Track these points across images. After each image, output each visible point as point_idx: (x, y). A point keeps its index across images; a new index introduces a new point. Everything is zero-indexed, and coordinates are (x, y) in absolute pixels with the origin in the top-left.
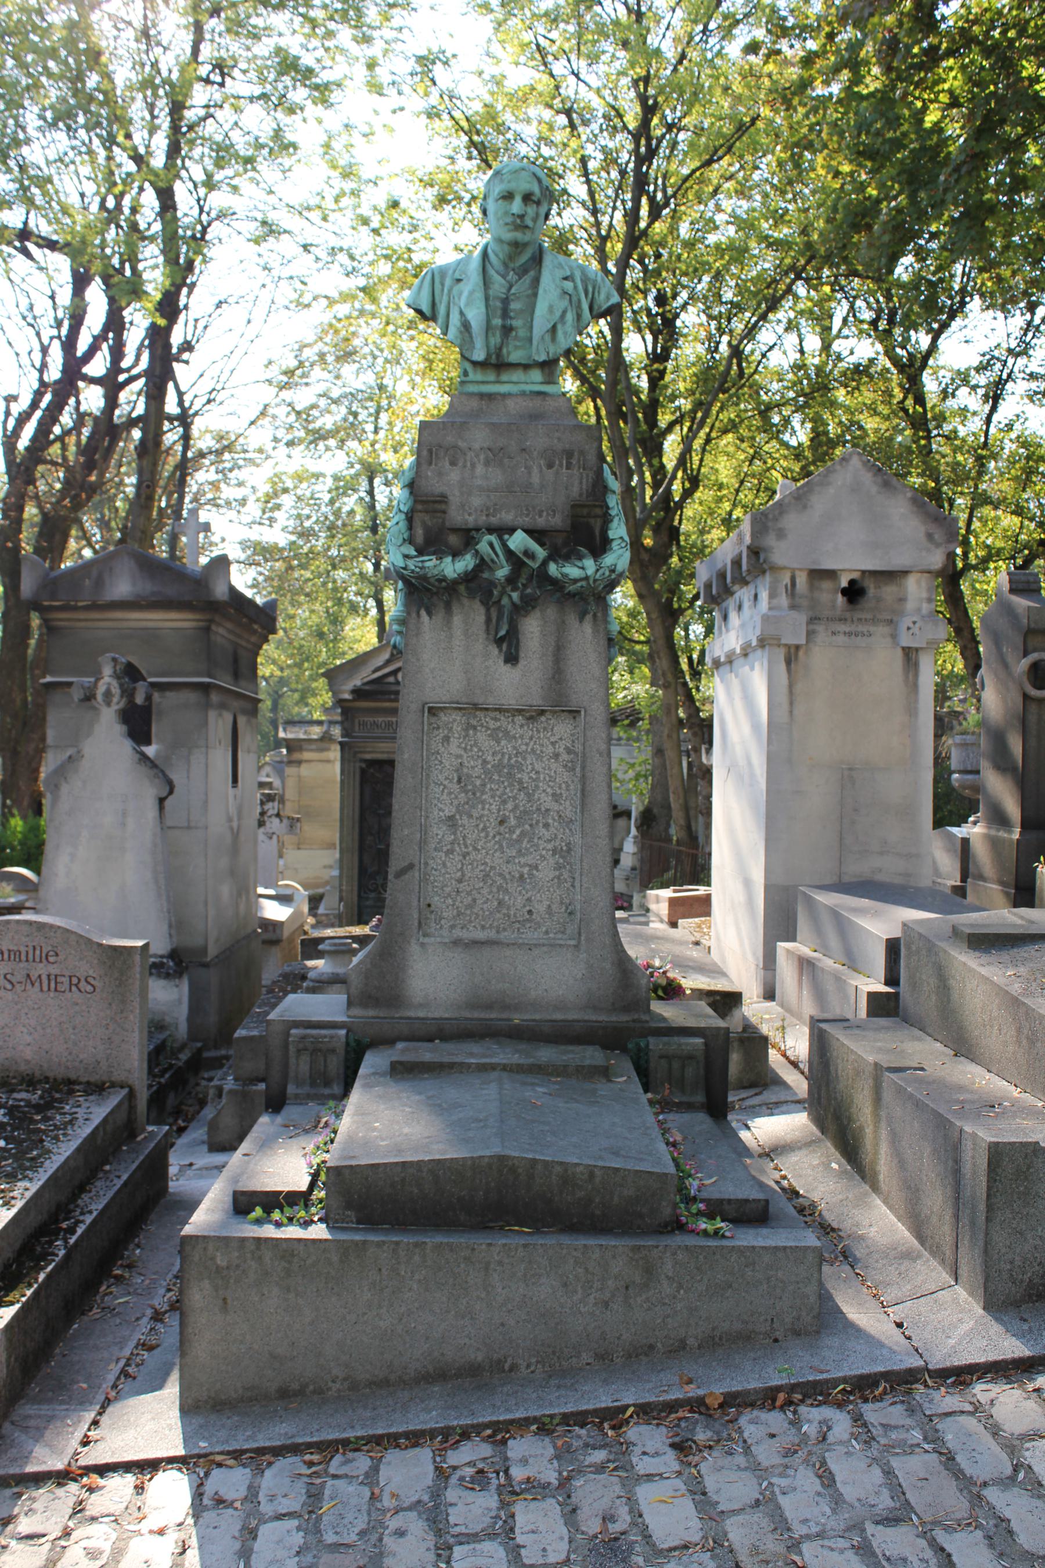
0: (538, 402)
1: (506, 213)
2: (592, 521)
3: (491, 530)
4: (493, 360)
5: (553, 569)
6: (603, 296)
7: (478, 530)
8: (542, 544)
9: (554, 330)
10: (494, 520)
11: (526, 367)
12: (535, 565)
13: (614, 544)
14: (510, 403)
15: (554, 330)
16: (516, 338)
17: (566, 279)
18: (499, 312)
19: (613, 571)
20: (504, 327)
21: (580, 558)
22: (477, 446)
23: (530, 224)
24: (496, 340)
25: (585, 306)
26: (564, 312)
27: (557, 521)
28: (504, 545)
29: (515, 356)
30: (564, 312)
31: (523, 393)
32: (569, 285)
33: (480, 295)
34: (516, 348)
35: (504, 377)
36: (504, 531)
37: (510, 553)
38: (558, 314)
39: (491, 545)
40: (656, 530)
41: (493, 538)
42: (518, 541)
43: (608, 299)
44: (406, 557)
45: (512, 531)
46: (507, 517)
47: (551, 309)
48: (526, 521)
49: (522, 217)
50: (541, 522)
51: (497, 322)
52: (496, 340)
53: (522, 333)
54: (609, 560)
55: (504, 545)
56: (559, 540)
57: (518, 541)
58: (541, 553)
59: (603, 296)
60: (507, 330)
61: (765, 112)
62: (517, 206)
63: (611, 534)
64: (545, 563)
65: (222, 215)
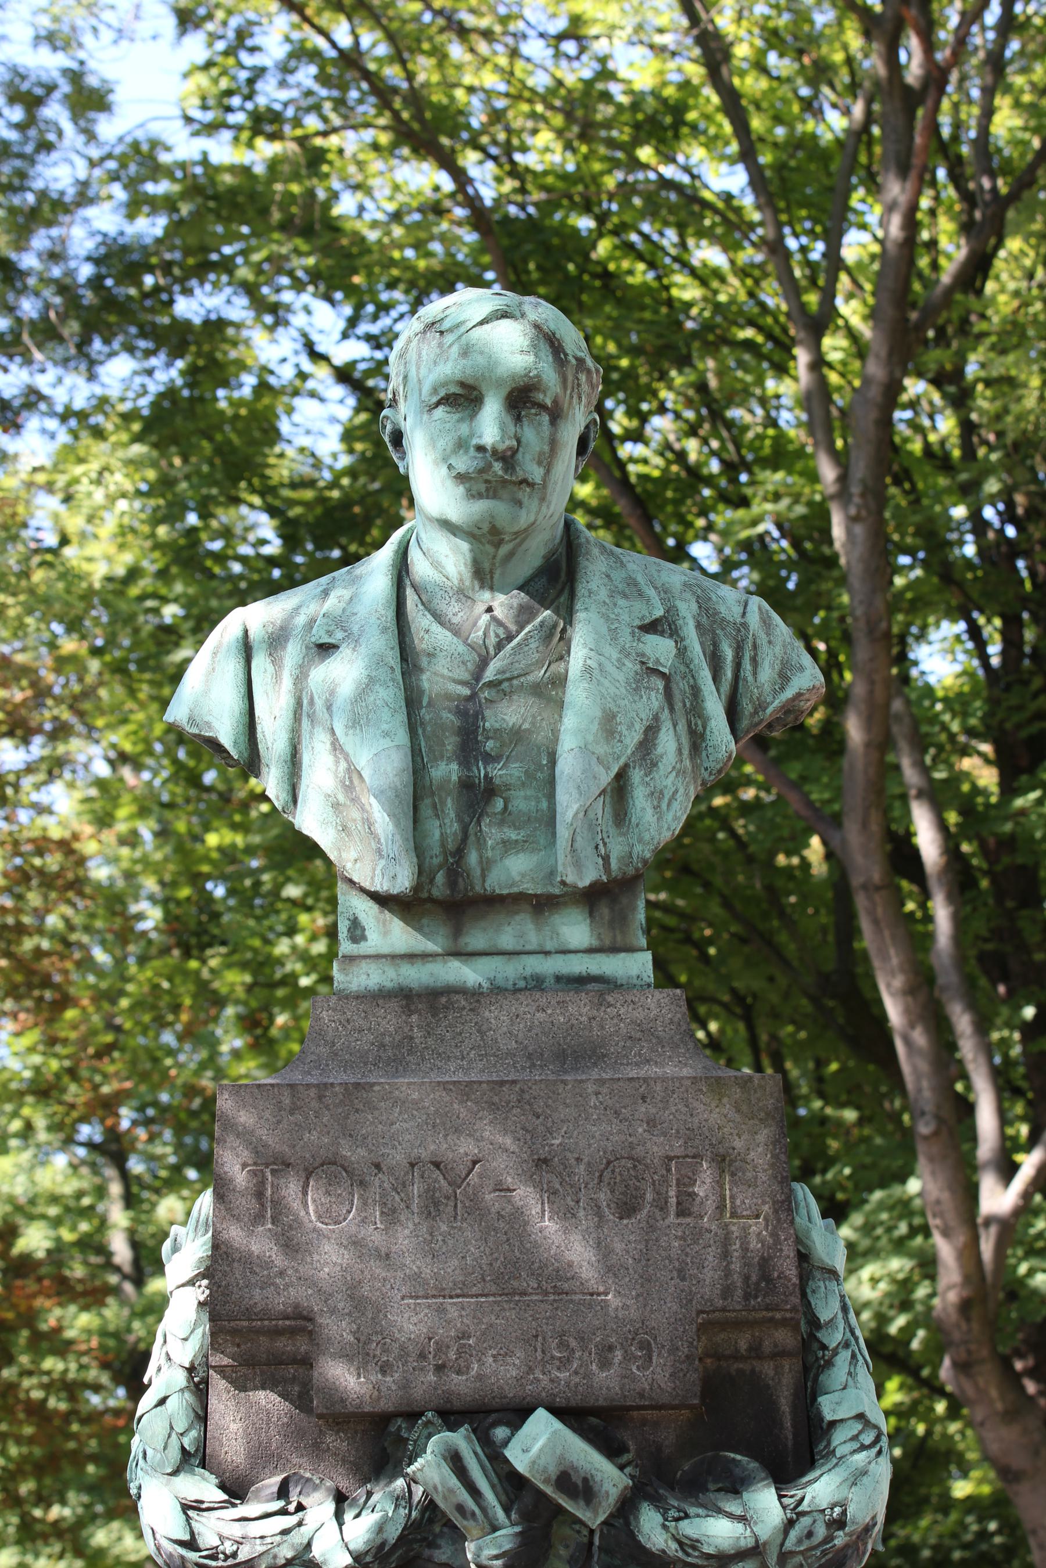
0: (580, 1007)
1: (461, 445)
2: (767, 1369)
3: (451, 1416)
4: (440, 887)
5: (652, 1529)
6: (767, 674)
7: (413, 1416)
8: (611, 1450)
9: (619, 789)
10: (461, 1385)
11: (542, 905)
12: (594, 1518)
13: (839, 1437)
14: (497, 1017)
15: (619, 789)
16: (505, 817)
17: (652, 627)
18: (451, 743)
19: (840, 1523)
20: (466, 785)
21: (736, 1486)
22: (397, 1157)
23: (536, 473)
24: (445, 826)
25: (715, 707)
26: (651, 732)
27: (658, 1376)
28: (495, 1457)
29: (515, 870)
30: (651, 732)
31: (536, 983)
32: (660, 649)
33: (388, 694)
34: (508, 846)
35: (476, 939)
36: (490, 1416)
37: (512, 1484)
38: (633, 738)
39: (455, 1461)
40: (987, 524)
41: (460, 1439)
42: (539, 1443)
43: (784, 679)
44: (190, 1507)
45: (518, 1414)
46: (500, 1372)
47: (609, 725)
48: (562, 1380)
49: (508, 458)
50: (607, 1382)
51: (446, 771)
52: (445, 826)
53: (522, 802)
54: (821, 1489)
55: (495, 1457)
56: (668, 1438)
57: (539, 1443)
58: (610, 1477)
59: (767, 674)
60: (477, 796)
61: (149, 974)
62: (490, 425)
63: (829, 1407)
64: (626, 1508)
65: (313, 394)
